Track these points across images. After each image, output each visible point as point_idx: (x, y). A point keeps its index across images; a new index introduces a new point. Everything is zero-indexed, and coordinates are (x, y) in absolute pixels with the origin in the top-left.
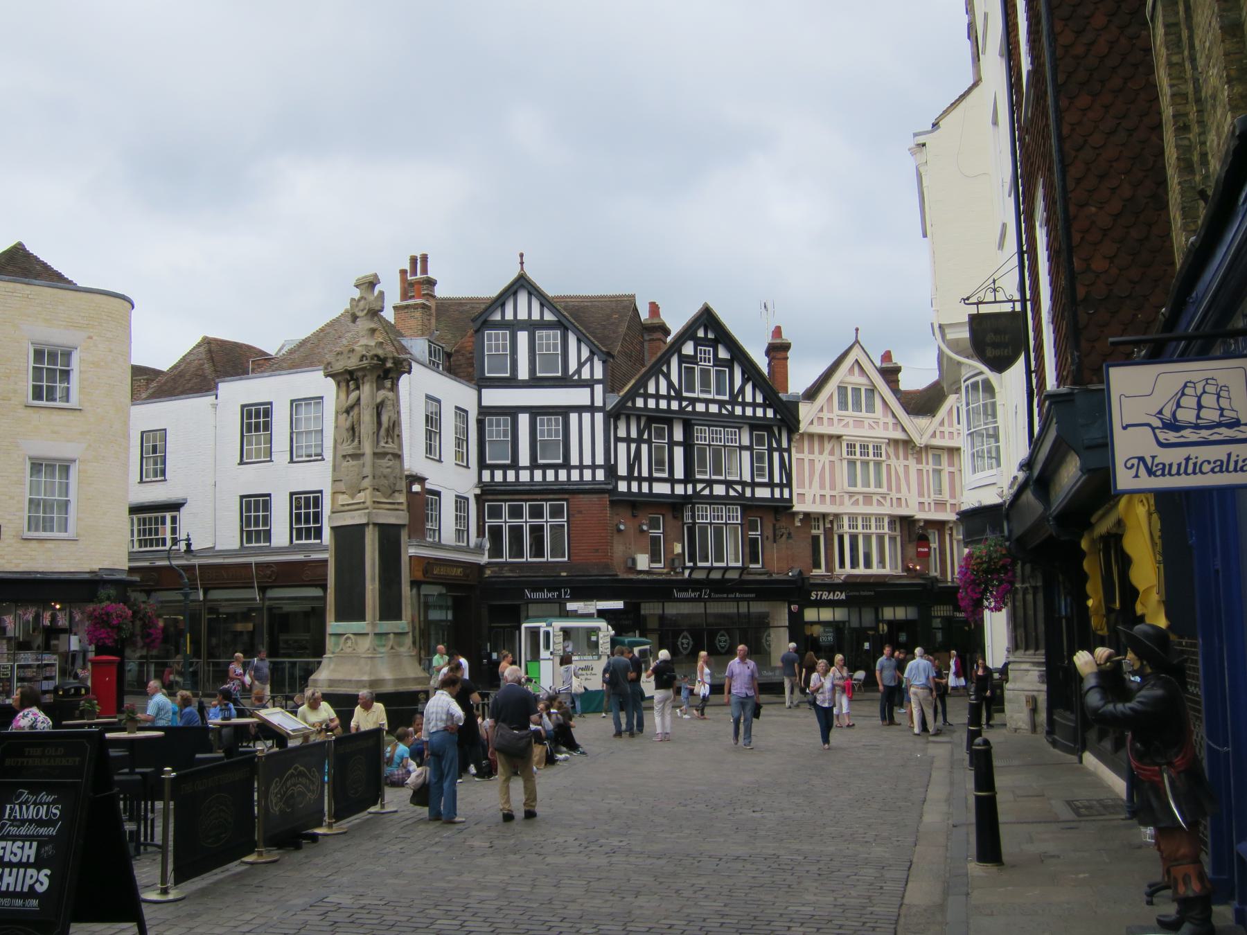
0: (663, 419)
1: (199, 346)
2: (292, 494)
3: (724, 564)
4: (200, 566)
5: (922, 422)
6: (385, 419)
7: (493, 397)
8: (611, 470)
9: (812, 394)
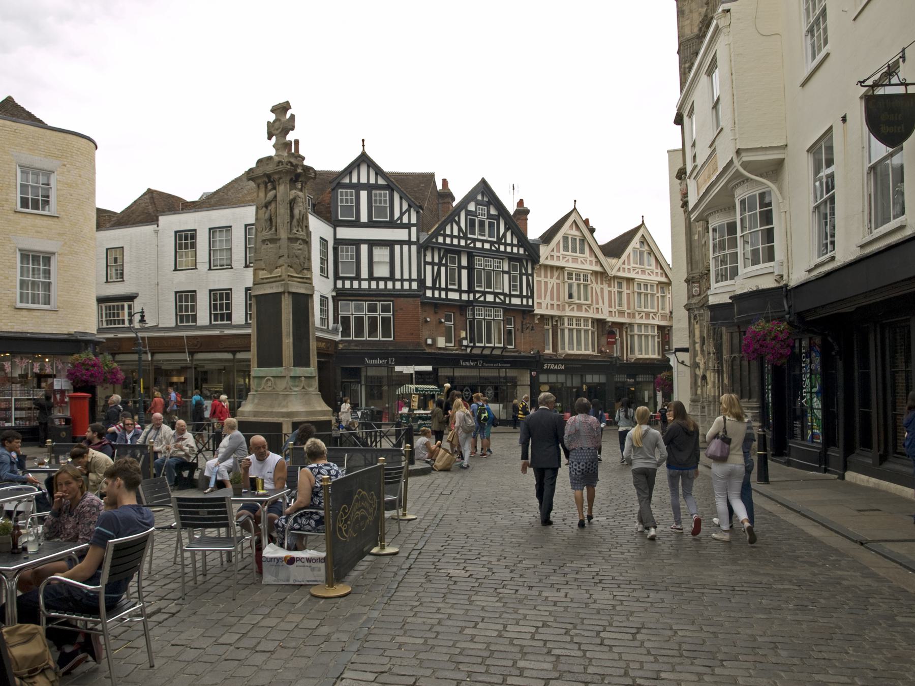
0: (452, 252)
1: (145, 194)
2: (210, 291)
3: (492, 345)
4: (148, 338)
5: (613, 261)
6: (296, 212)
7: (345, 233)
8: (421, 282)
9: (547, 237)
